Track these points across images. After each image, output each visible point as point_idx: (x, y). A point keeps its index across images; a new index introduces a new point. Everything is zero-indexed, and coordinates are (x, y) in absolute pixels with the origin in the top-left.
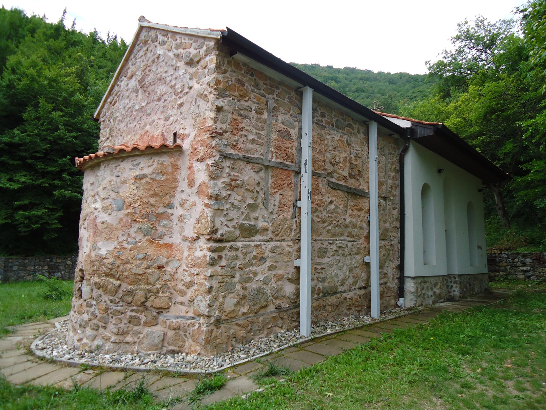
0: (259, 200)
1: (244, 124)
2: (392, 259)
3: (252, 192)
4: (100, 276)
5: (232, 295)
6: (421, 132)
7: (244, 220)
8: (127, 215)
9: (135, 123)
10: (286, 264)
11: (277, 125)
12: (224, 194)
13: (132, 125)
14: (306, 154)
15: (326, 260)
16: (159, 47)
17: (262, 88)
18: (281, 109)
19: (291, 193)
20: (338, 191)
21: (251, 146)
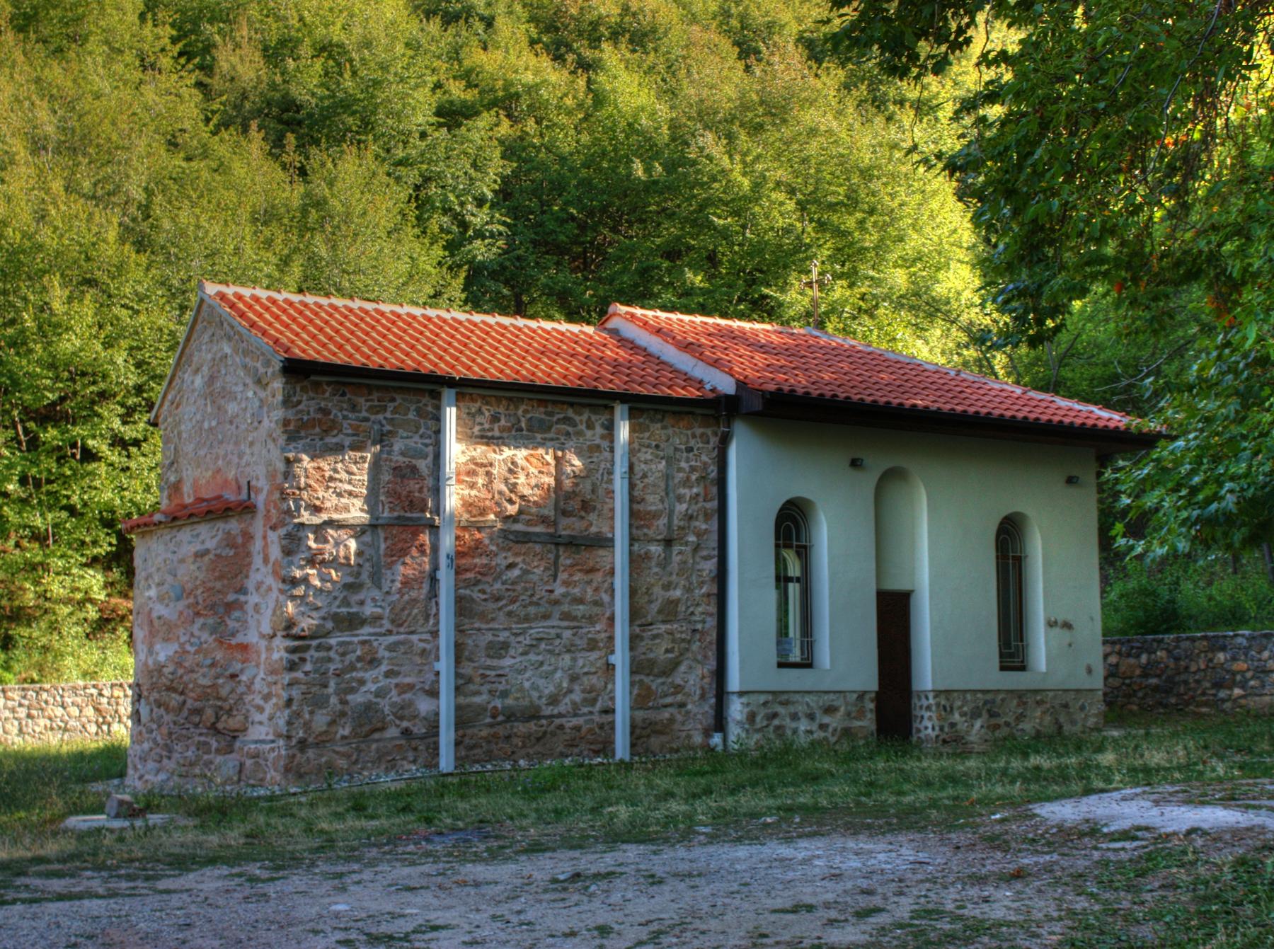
2: (699, 657)
7: (339, 607)
8: (188, 607)
13: (202, 453)
15: (507, 662)
20: (530, 545)
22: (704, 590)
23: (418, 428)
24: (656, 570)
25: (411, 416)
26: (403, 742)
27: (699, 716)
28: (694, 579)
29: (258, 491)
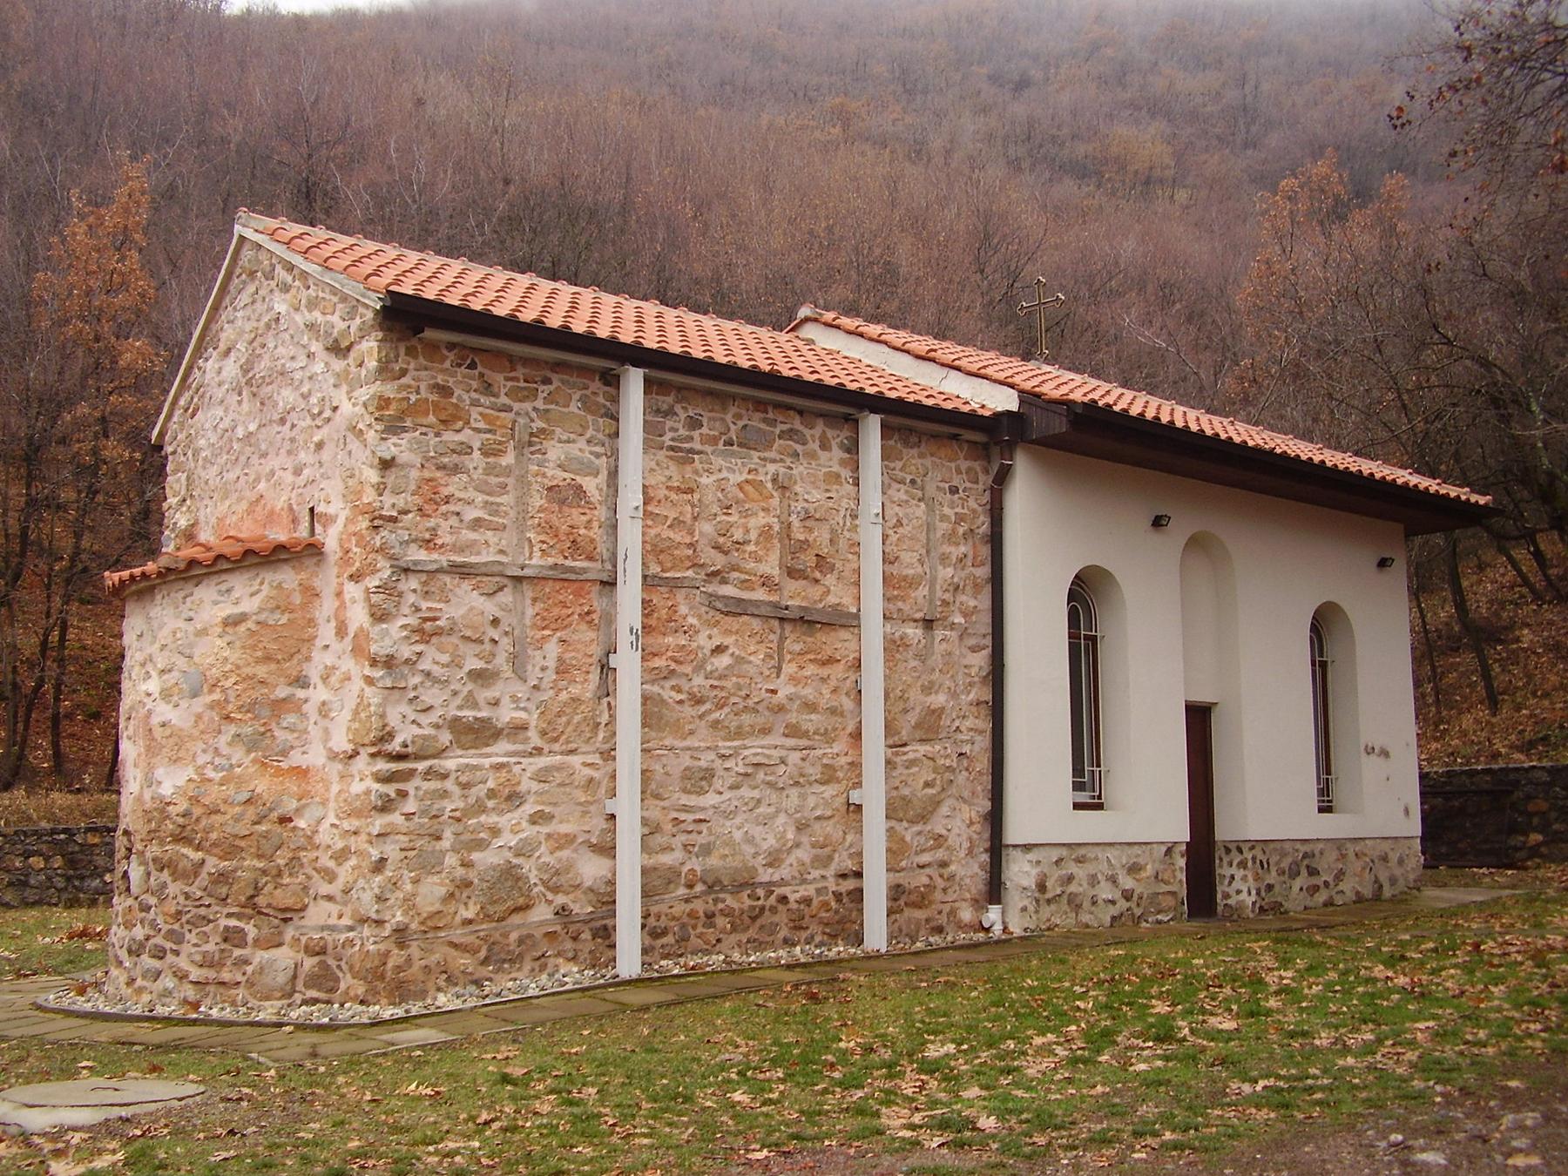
0: (501, 660)
1: (453, 486)
2: (966, 794)
3: (480, 641)
4: (162, 843)
5: (436, 879)
6: (1040, 423)
7: (460, 708)
8: (211, 706)
9: (238, 472)
10: (580, 808)
11: (544, 476)
12: (406, 652)
13: (231, 476)
14: (631, 538)
15: (711, 799)
16: (277, 296)
17: (503, 391)
18: (558, 430)
19: (592, 635)
21: (472, 536)
22: (971, 696)
23: (585, 428)
24: (913, 663)
25: (574, 407)
26: (558, 928)
27: (968, 881)
28: (960, 679)
29: (329, 520)
